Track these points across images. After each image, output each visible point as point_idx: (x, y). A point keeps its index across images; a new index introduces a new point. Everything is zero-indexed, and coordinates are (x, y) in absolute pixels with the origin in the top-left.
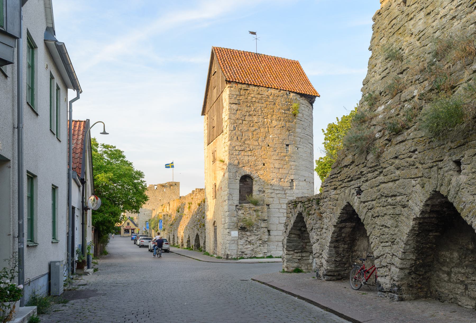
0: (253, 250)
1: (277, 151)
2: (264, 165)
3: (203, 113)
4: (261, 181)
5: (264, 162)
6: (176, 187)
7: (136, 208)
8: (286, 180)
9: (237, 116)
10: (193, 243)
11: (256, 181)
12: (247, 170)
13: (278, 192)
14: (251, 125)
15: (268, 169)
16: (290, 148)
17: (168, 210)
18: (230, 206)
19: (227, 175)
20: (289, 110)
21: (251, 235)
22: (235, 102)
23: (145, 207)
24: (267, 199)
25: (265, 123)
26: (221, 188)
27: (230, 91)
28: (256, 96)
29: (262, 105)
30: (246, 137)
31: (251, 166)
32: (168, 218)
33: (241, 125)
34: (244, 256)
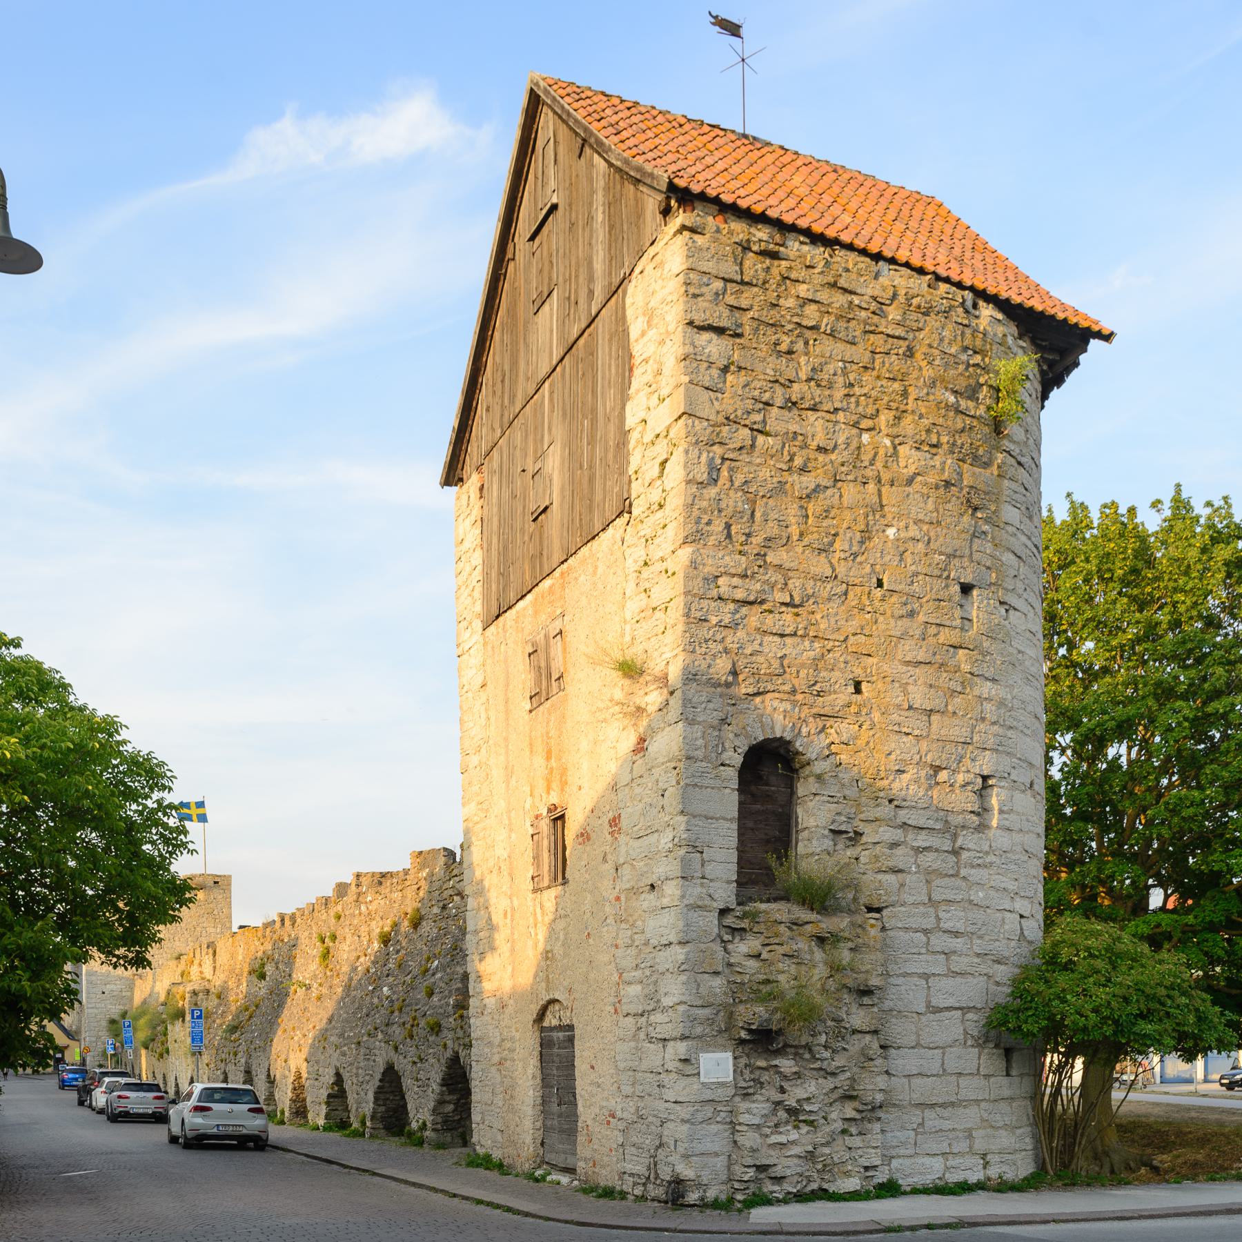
0: (810, 1156)
1: (922, 618)
3: (452, 475)
4: (845, 777)
5: (858, 672)
6: (217, 893)
7: (133, 943)
8: (960, 778)
9: (729, 403)
10: (362, 1102)
11: (819, 777)
12: (776, 716)
13: (922, 840)
14: (798, 462)
15: (876, 716)
16: (978, 603)
17: (208, 972)
18: (694, 915)
19: (668, 742)
20: (972, 393)
21: (798, 1075)
22: (715, 326)
24: (870, 876)
25: (866, 458)
26: (614, 822)
27: (693, 252)
28: (823, 296)
29: (849, 352)
30: (772, 529)
31: (794, 691)
32: (210, 1004)
33: (744, 457)
34: (769, 1187)
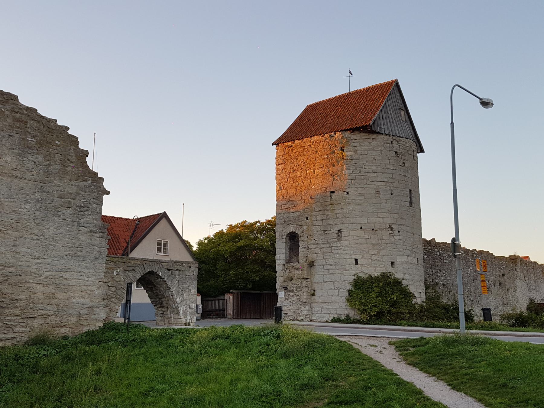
2: (307, 219)
13: (322, 246)
23: (373, 268)
29: (304, 157)
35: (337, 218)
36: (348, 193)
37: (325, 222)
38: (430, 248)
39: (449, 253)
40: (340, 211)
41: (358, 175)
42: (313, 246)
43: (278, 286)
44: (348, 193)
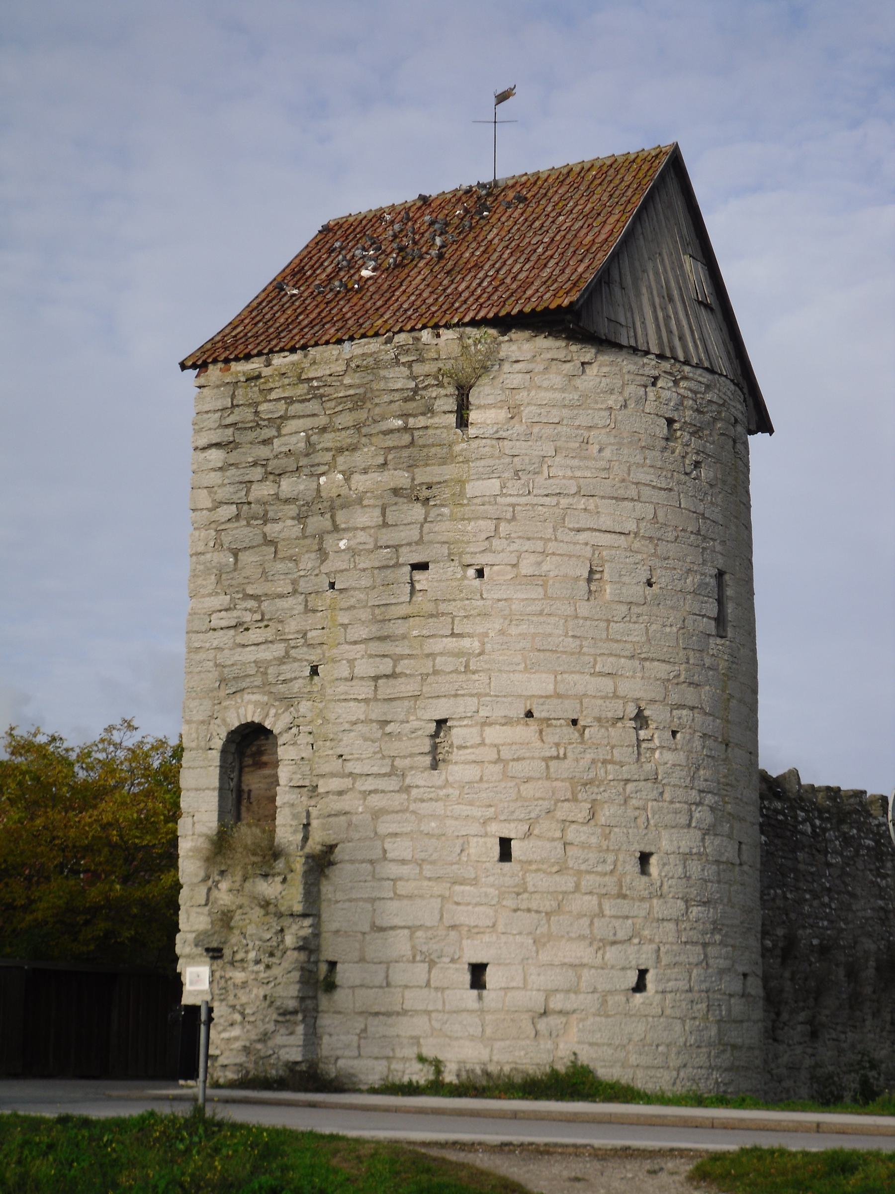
13: (369, 784)
35: (436, 672)
36: (480, 573)
37: (386, 689)
38: (779, 805)
39: (845, 828)
40: (451, 643)
41: (523, 500)
42: (335, 784)
43: (183, 944)
44: (480, 573)
